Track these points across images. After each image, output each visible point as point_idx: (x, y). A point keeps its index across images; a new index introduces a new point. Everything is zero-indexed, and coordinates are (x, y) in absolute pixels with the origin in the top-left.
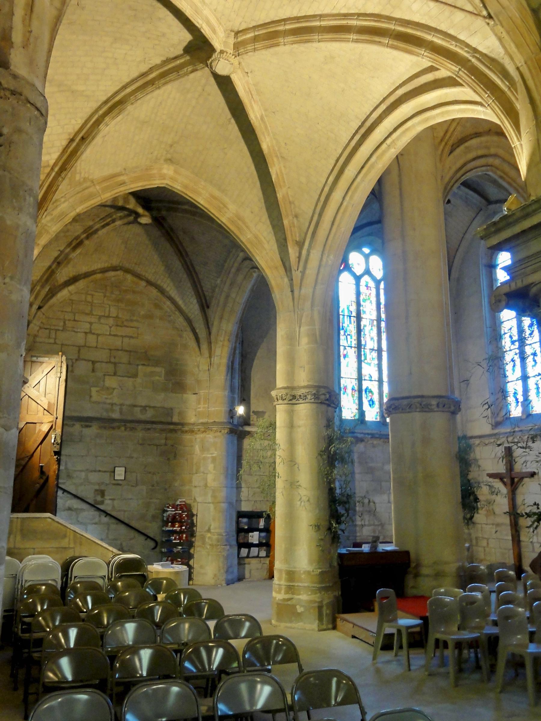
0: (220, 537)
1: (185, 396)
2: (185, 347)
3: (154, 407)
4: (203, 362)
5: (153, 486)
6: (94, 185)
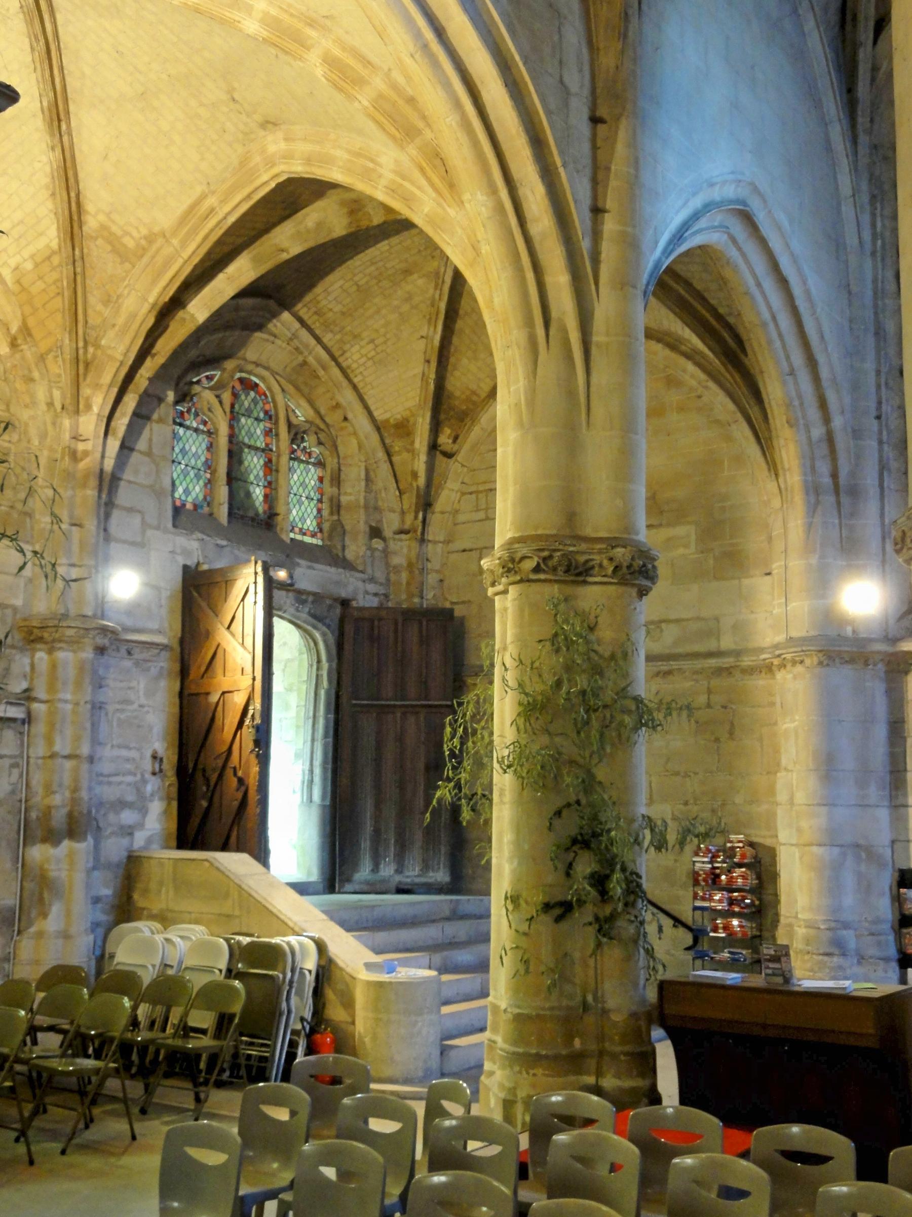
0: (812, 932)
1: (746, 582)
2: (739, 460)
3: (678, 621)
4: (772, 486)
5: (686, 803)
6: (167, 241)
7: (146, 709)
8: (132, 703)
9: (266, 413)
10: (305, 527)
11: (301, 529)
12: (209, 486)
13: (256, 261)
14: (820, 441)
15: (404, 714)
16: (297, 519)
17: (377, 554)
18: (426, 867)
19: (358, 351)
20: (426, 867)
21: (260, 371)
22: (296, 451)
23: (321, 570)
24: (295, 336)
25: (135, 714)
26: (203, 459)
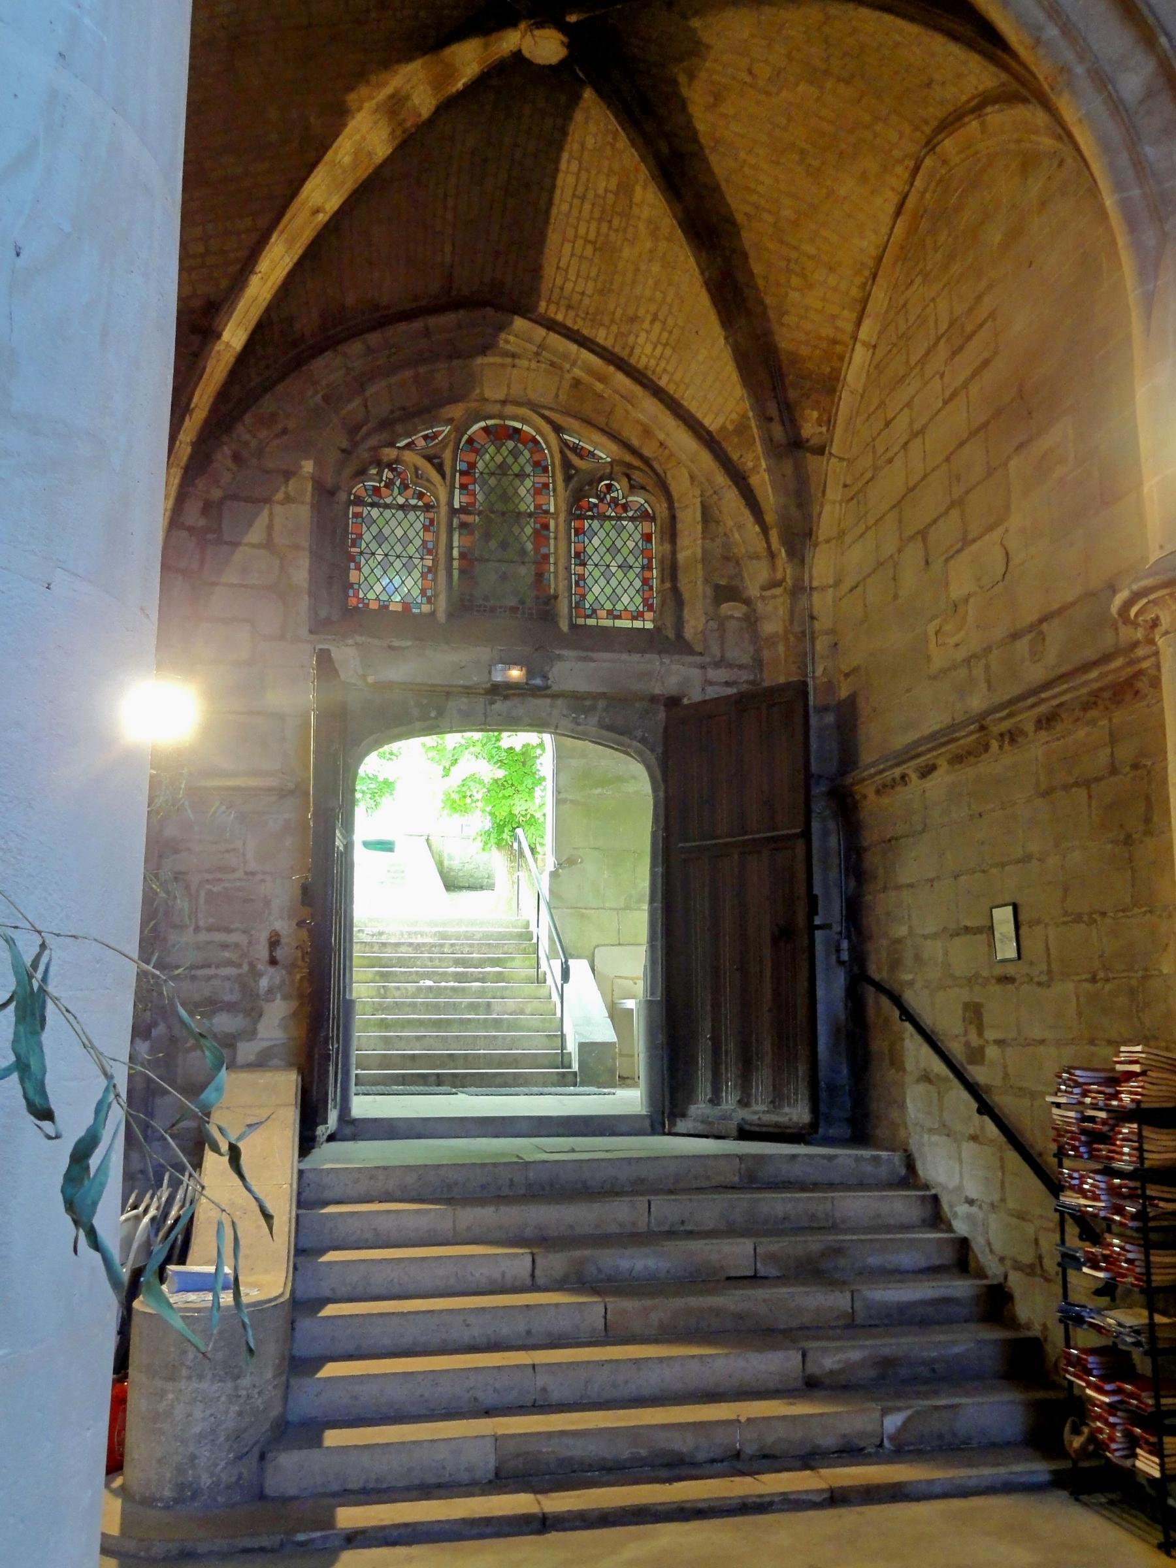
7: (259, 877)
8: (233, 871)
9: (537, 464)
10: (619, 607)
11: (610, 612)
12: (430, 576)
13: (291, 243)
14: (1149, 94)
16: (602, 599)
17: (732, 625)
18: (778, 1099)
20: (778, 1099)
21: (510, 409)
22: (596, 505)
24: (542, 346)
25: (238, 884)
26: (418, 542)
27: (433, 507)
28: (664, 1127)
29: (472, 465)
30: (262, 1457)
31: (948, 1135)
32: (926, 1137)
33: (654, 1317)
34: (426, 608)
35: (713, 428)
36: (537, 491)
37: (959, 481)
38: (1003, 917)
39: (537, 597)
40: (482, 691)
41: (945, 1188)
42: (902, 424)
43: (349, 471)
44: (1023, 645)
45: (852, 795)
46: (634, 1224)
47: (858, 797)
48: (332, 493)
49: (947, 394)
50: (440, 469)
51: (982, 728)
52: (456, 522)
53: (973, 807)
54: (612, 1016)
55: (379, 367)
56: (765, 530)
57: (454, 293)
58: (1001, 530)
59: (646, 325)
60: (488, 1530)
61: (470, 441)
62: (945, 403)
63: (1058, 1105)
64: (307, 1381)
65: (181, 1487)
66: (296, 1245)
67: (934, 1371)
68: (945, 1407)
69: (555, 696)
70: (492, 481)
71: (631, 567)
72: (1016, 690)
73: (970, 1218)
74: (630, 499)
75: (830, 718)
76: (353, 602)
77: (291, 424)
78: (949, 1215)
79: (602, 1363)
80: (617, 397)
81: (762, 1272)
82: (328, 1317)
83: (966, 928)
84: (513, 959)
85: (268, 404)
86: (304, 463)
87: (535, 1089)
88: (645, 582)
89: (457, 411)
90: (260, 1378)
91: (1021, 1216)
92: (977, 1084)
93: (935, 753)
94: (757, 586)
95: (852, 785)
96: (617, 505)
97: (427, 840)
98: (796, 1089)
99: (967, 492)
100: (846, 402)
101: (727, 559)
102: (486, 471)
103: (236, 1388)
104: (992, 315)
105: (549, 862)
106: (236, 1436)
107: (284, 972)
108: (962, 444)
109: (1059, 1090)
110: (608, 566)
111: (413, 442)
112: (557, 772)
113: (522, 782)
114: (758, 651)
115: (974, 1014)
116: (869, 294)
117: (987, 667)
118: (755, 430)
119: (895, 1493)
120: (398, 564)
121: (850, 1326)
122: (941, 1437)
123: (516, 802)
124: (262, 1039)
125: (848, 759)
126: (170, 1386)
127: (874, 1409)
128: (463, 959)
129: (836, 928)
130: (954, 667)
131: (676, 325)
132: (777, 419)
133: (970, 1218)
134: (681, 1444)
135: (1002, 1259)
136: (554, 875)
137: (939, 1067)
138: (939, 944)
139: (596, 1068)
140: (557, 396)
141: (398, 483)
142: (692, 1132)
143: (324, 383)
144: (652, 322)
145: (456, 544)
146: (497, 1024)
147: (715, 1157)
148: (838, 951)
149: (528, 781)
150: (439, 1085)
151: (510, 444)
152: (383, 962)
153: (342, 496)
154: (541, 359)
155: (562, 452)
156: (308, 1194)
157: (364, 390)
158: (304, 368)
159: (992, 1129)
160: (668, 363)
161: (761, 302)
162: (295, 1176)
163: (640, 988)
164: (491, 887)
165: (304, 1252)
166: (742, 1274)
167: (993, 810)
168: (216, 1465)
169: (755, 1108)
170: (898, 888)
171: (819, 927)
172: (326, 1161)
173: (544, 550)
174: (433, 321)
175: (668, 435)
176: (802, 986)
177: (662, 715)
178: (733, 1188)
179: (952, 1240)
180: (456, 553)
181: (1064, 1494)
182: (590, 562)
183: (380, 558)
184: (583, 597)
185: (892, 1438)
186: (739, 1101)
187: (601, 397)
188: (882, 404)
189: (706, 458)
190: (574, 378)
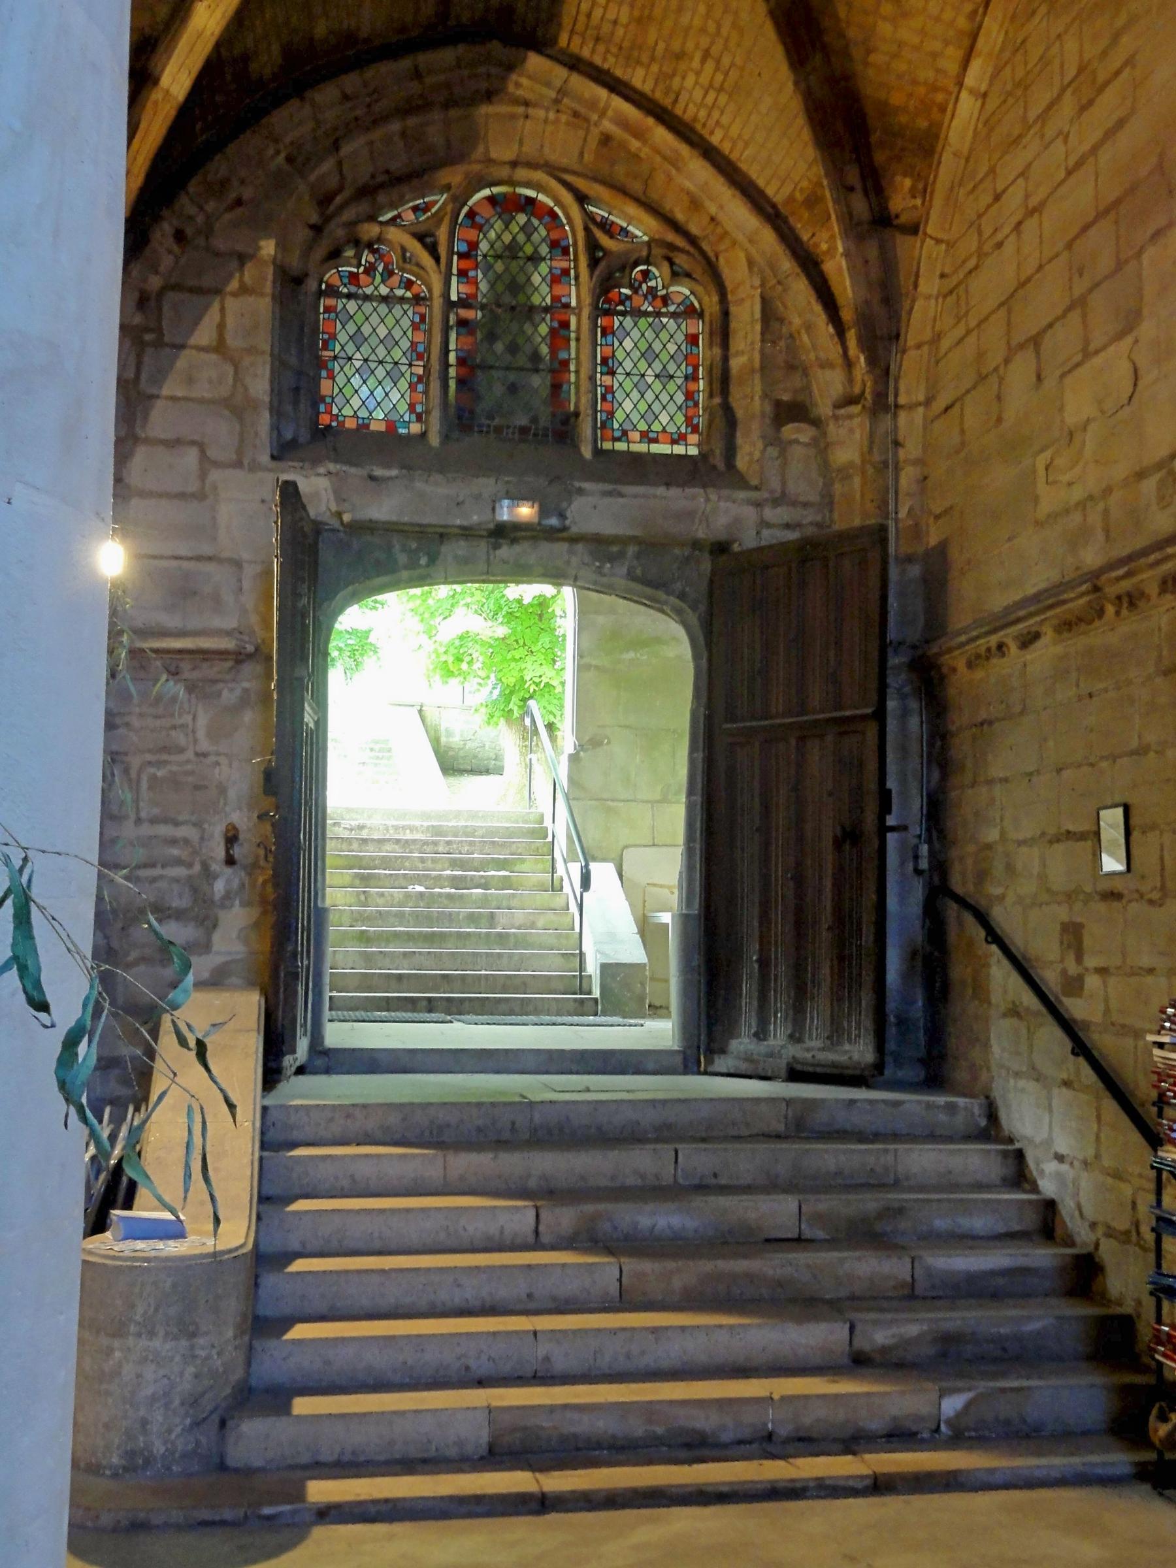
7: (212, 758)
8: (182, 750)
9: (554, 245)
10: (656, 427)
15: (802, 739)
16: (635, 417)
18: (836, 1034)
19: (696, 83)
20: (836, 1034)
21: (522, 173)
22: (628, 298)
23: (636, 496)
25: (189, 767)
26: (405, 344)
27: (424, 299)
28: (699, 1066)
29: (473, 246)
30: (223, 1423)
31: (1037, 1080)
32: (1012, 1081)
33: (677, 1283)
34: (416, 428)
35: (778, 199)
36: (556, 279)
37: (1081, 275)
38: (1111, 820)
39: (554, 415)
40: (485, 533)
41: (1031, 1141)
42: (1014, 200)
43: (320, 252)
44: (1150, 485)
45: (938, 668)
46: (657, 1176)
47: (945, 670)
48: (298, 281)
49: (1071, 162)
50: (433, 250)
51: (1096, 589)
52: (452, 319)
53: (1082, 685)
54: (642, 932)
55: (356, 119)
56: (841, 331)
57: (452, 22)
58: (1129, 340)
59: (696, 64)
60: (479, 1509)
61: (471, 214)
62: (1069, 173)
63: (1161, 1046)
64: (272, 1343)
65: (131, 1454)
66: (259, 1192)
67: (1004, 1349)
68: (1012, 1390)
69: (574, 540)
70: (499, 266)
71: (672, 377)
72: (1140, 543)
73: (1059, 1177)
74: (672, 289)
75: (915, 571)
76: (324, 419)
77: (247, 193)
78: (1035, 1173)
79: (614, 1332)
80: (658, 159)
81: (808, 1233)
82: (299, 1273)
83: (1068, 832)
84: (523, 861)
85: (218, 167)
86: (262, 243)
87: (547, 1018)
88: (689, 396)
89: (454, 176)
90: (220, 1341)
91: (1117, 1175)
92: (1075, 1021)
93: (1038, 619)
94: (829, 403)
95: (940, 654)
96: (655, 297)
97: (420, 711)
98: (859, 1024)
99: (1090, 290)
100: (947, 168)
101: (791, 367)
102: (491, 253)
103: (192, 1347)
104: (1129, 62)
105: (568, 741)
106: (194, 1401)
107: (243, 874)
108: (1085, 229)
109: (1163, 1027)
110: (643, 376)
111: (399, 216)
112: (581, 628)
113: (537, 640)
114: (828, 485)
115: (1073, 934)
116: (980, 27)
117: (1106, 512)
118: (830, 205)
119: (949, 1482)
120: (380, 372)
121: (910, 1295)
122: (1008, 1422)
123: (529, 665)
124: (218, 953)
125: (935, 622)
126: (116, 1343)
127: (931, 1388)
128: (460, 859)
129: (915, 830)
130: (1067, 511)
131: (732, 64)
132: (858, 186)
133: (1059, 1177)
134: (704, 1422)
135: (1093, 1225)
136: (574, 759)
137: (1029, 999)
138: (1036, 852)
139: (621, 992)
140: (581, 154)
141: (380, 269)
142: (732, 1071)
143: (287, 140)
144: (704, 60)
145: (452, 346)
146: (502, 939)
147: (757, 1101)
148: (916, 857)
149: (545, 639)
150: (430, 1011)
151: (522, 218)
152: (364, 863)
153: (311, 285)
154: (562, 107)
155: (587, 229)
156: (272, 1135)
157: (337, 149)
158: (264, 121)
159: (1088, 1074)
160: (722, 113)
161: (842, 35)
162: (258, 1115)
163: (674, 898)
164: (499, 771)
165: (268, 1200)
166: (784, 1236)
167: (1106, 690)
168: (170, 1431)
169: (810, 1044)
170: (990, 782)
171: (892, 829)
172: (294, 1097)
173: (563, 355)
174: (424, 59)
175: (721, 207)
176: (872, 897)
177: (706, 566)
178: (779, 1137)
179: (1037, 1201)
180: (452, 358)
181: (1147, 1487)
182: (620, 370)
183: (358, 364)
184: (611, 414)
185: (949, 1422)
186: (791, 1036)
187: (636, 157)
188: (992, 171)
189: (768, 236)
190: (602, 133)
